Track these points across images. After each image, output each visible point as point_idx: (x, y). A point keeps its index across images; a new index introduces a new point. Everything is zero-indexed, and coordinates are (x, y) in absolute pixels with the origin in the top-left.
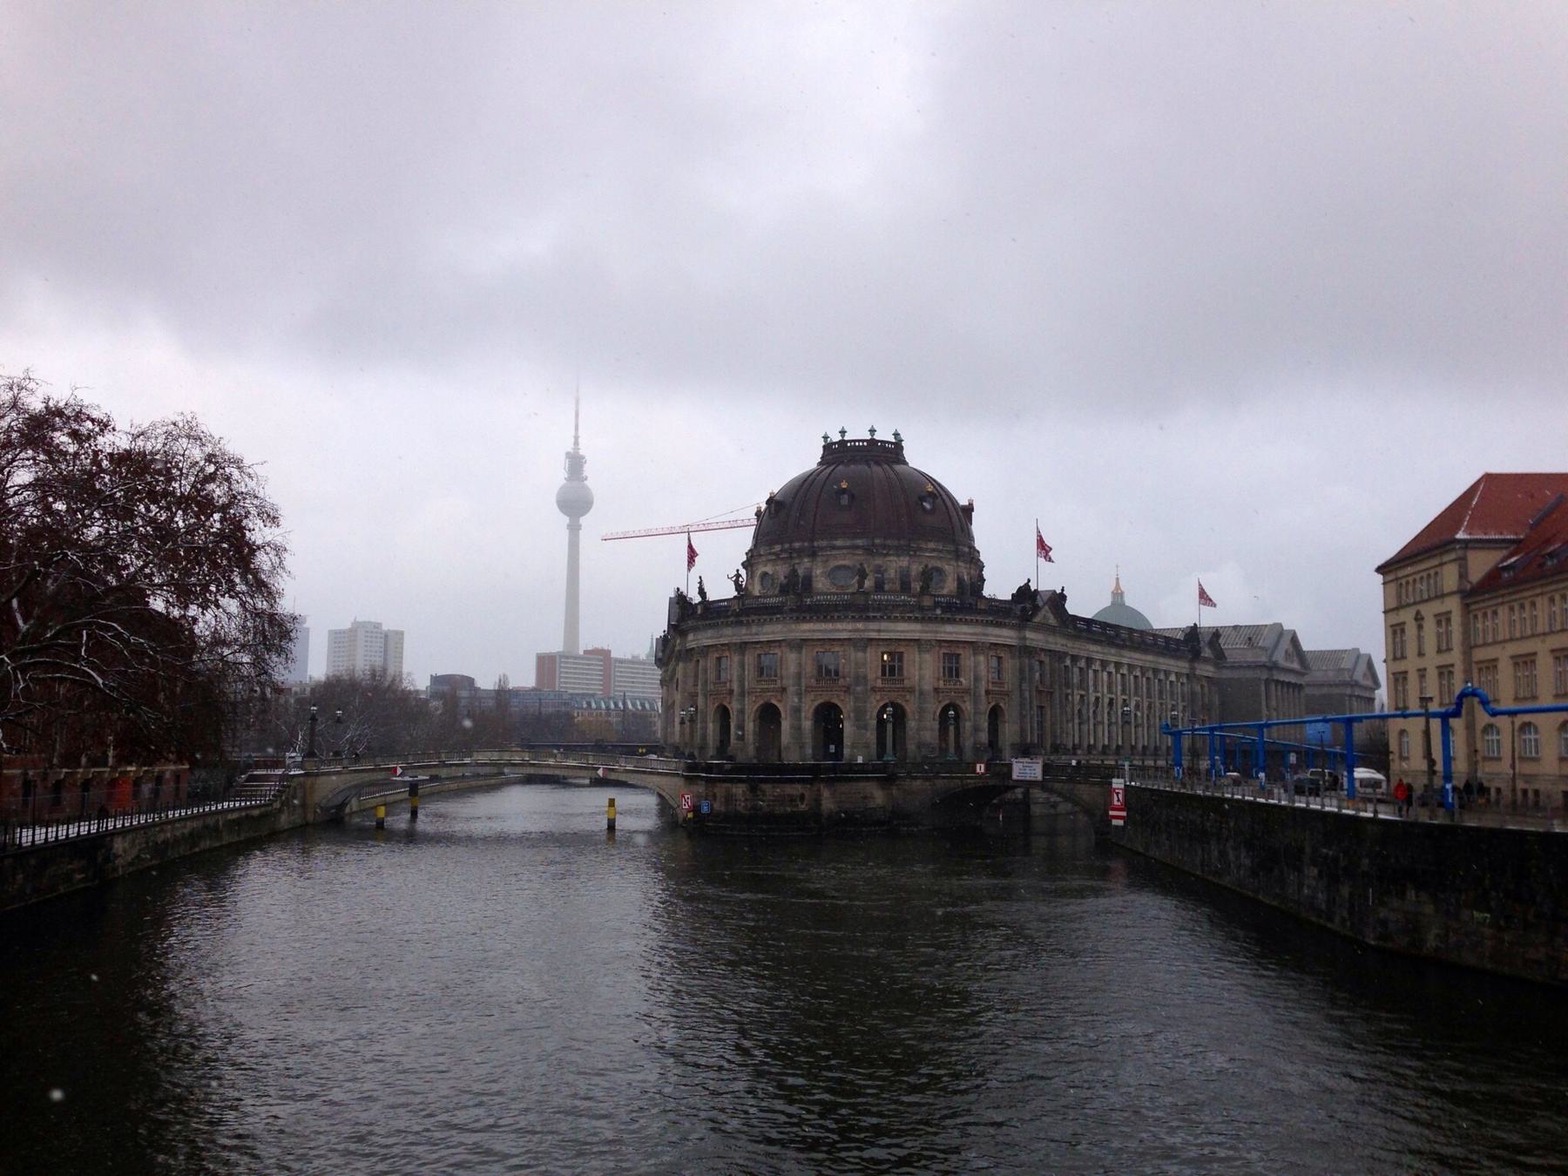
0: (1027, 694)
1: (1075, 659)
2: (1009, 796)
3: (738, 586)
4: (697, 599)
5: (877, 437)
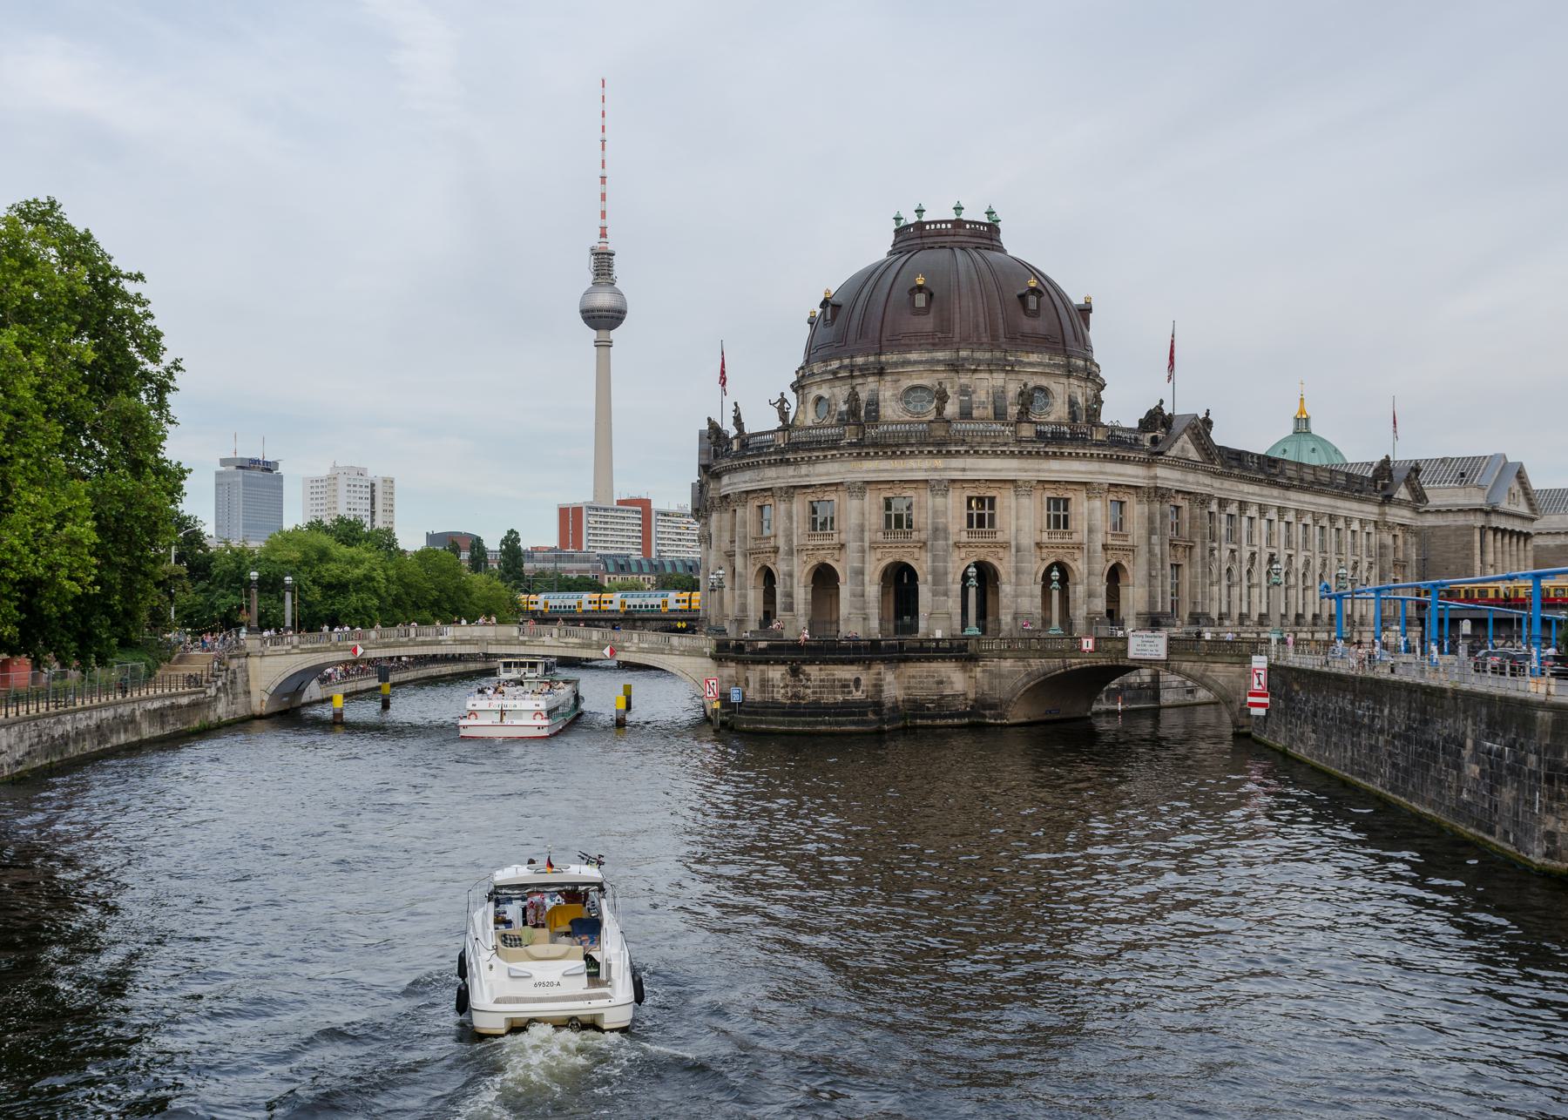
0: (1157, 550)
2: (1133, 679)
5: (965, 216)
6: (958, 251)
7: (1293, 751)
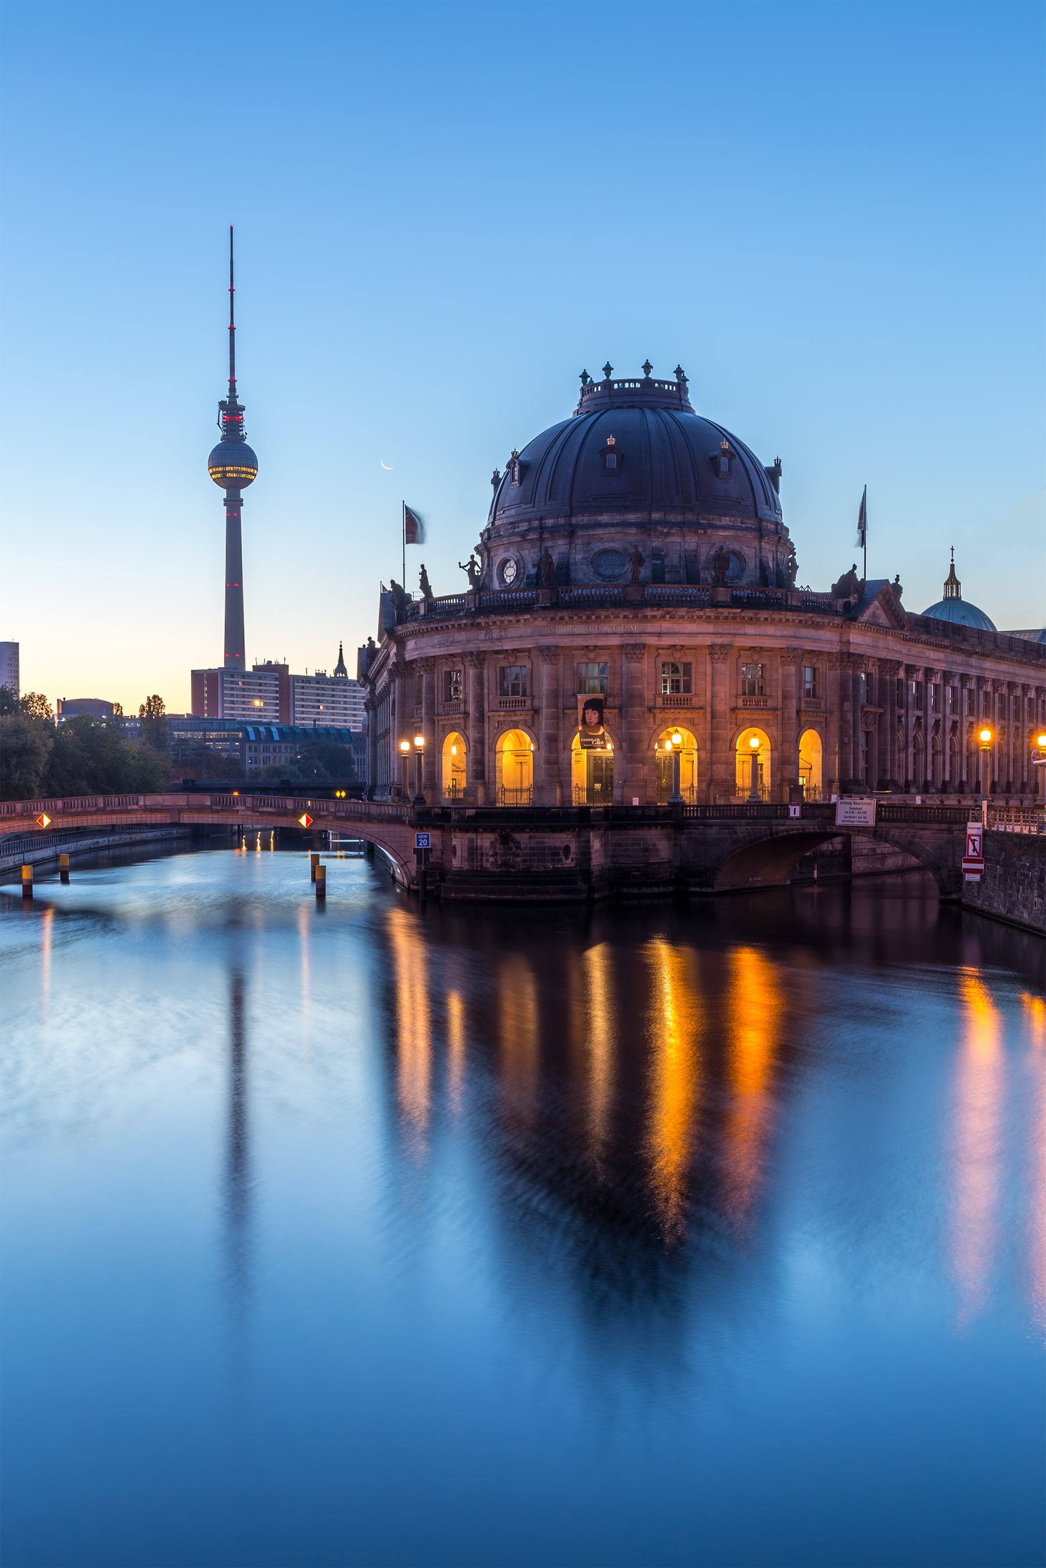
0: (850, 717)
1: (910, 669)
2: (826, 847)
3: (473, 579)
4: (418, 595)
6: (648, 412)
7: (1015, 916)
